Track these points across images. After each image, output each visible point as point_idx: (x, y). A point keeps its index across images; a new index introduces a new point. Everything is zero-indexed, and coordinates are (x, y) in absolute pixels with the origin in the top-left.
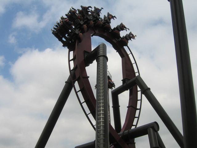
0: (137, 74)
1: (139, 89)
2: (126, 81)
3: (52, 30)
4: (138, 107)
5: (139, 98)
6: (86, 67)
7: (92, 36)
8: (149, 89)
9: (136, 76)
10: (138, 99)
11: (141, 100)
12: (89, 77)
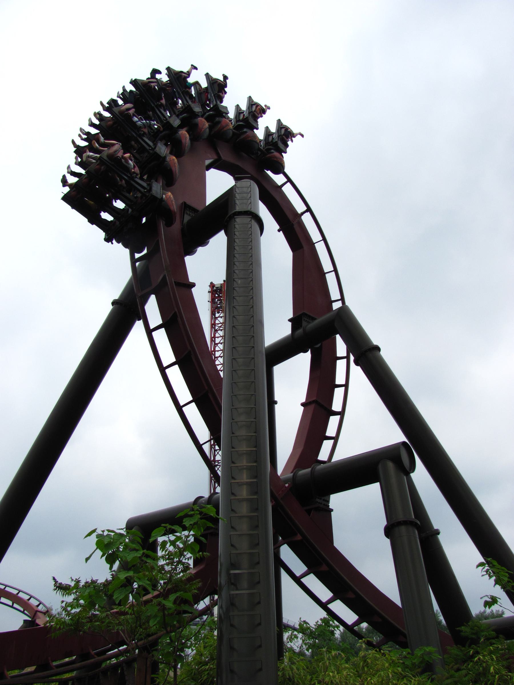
2: (304, 324)
3: (73, 142)
4: (336, 406)
5: (340, 379)
8: (378, 349)
10: (332, 299)
11: (346, 386)
12: (193, 285)
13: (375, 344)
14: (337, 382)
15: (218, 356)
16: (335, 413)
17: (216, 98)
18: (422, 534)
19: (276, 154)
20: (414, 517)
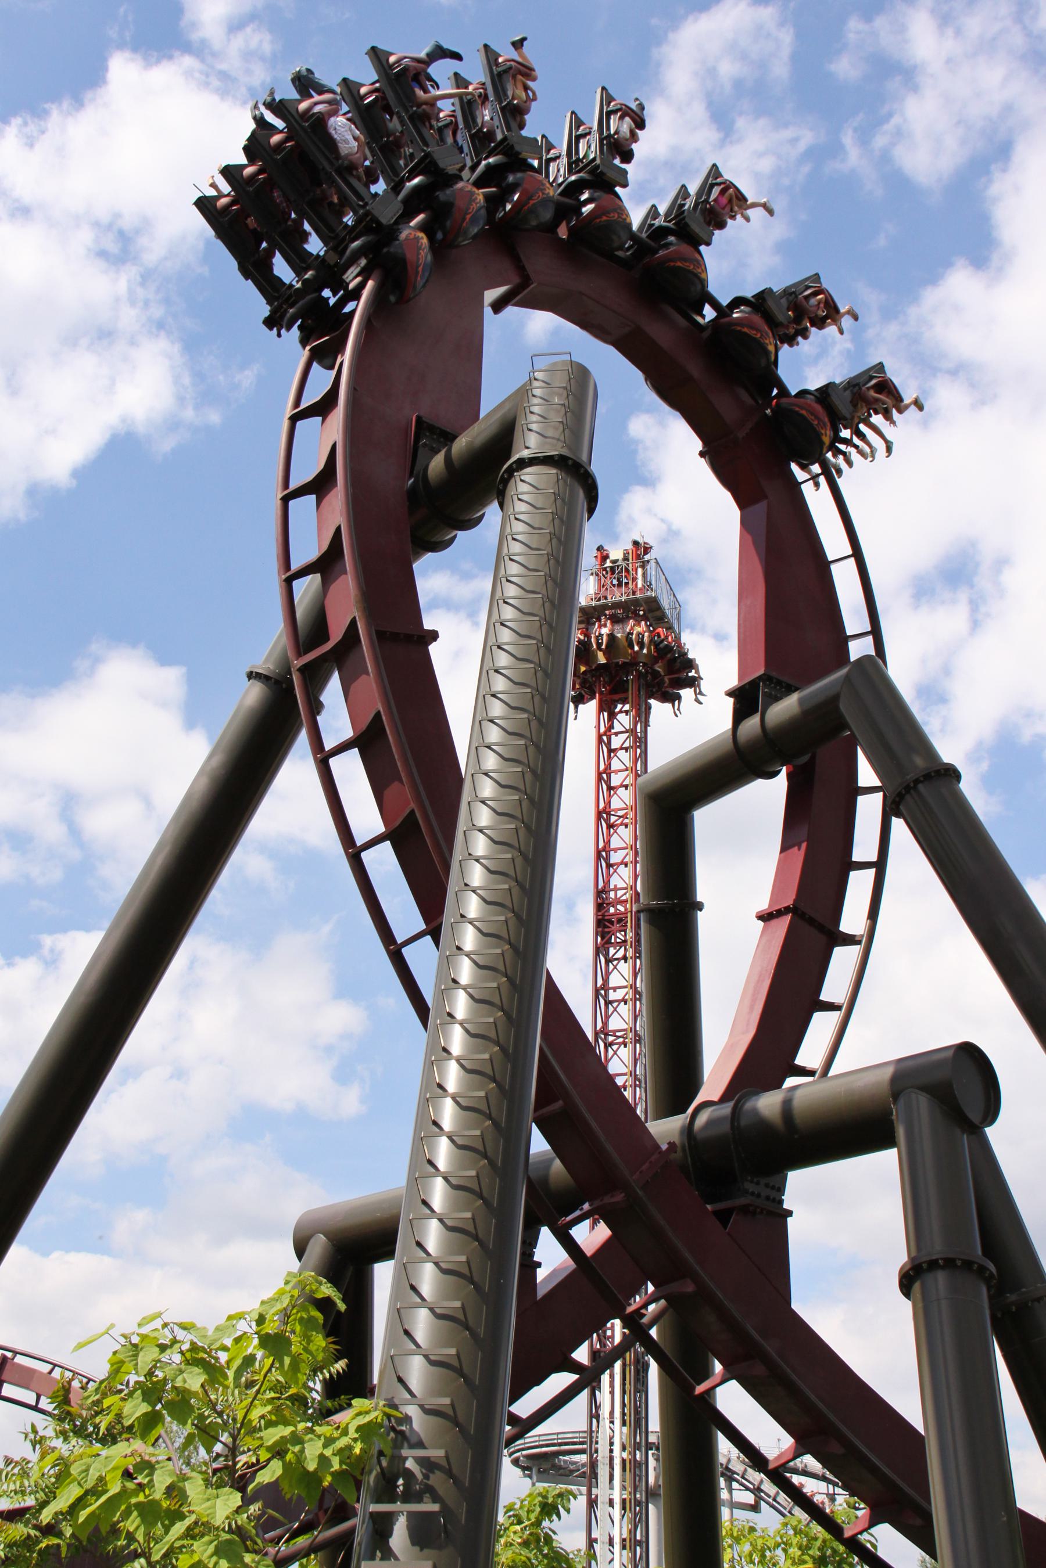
0: (859, 649)
1: (866, 775)
5: (864, 848)
6: (418, 555)
7: (498, 306)
9: (854, 656)
11: (880, 866)
13: (945, 762)
14: (857, 856)
15: (618, 747)
16: (850, 940)
17: (508, 114)
18: (1008, 1295)
19: (686, 249)
20: (980, 1252)
